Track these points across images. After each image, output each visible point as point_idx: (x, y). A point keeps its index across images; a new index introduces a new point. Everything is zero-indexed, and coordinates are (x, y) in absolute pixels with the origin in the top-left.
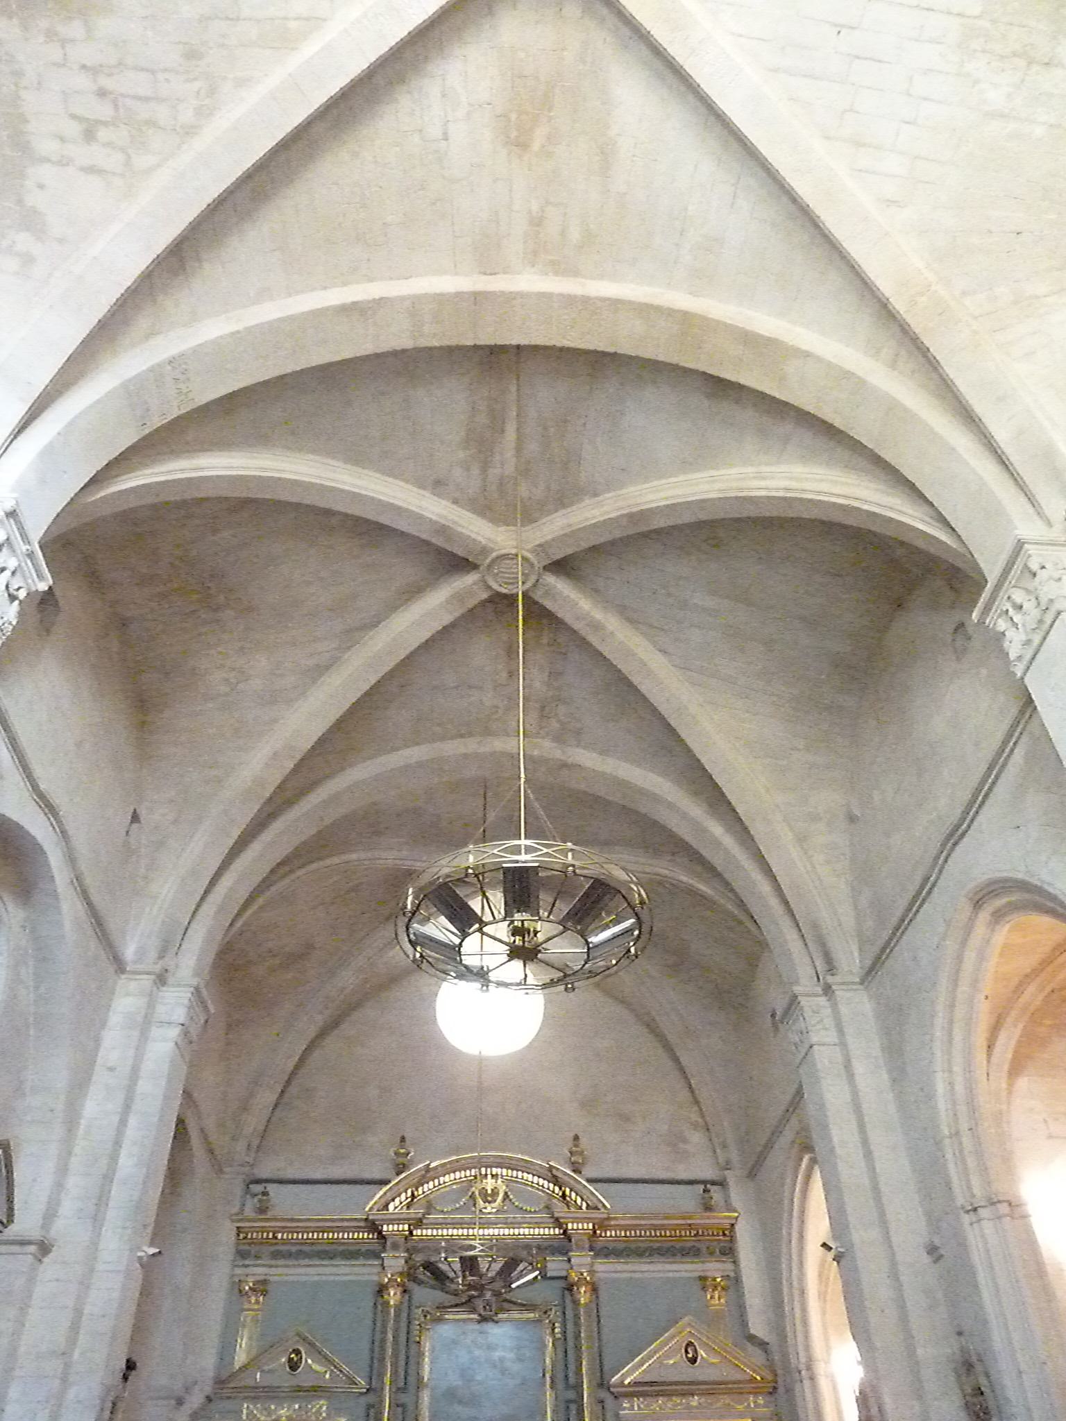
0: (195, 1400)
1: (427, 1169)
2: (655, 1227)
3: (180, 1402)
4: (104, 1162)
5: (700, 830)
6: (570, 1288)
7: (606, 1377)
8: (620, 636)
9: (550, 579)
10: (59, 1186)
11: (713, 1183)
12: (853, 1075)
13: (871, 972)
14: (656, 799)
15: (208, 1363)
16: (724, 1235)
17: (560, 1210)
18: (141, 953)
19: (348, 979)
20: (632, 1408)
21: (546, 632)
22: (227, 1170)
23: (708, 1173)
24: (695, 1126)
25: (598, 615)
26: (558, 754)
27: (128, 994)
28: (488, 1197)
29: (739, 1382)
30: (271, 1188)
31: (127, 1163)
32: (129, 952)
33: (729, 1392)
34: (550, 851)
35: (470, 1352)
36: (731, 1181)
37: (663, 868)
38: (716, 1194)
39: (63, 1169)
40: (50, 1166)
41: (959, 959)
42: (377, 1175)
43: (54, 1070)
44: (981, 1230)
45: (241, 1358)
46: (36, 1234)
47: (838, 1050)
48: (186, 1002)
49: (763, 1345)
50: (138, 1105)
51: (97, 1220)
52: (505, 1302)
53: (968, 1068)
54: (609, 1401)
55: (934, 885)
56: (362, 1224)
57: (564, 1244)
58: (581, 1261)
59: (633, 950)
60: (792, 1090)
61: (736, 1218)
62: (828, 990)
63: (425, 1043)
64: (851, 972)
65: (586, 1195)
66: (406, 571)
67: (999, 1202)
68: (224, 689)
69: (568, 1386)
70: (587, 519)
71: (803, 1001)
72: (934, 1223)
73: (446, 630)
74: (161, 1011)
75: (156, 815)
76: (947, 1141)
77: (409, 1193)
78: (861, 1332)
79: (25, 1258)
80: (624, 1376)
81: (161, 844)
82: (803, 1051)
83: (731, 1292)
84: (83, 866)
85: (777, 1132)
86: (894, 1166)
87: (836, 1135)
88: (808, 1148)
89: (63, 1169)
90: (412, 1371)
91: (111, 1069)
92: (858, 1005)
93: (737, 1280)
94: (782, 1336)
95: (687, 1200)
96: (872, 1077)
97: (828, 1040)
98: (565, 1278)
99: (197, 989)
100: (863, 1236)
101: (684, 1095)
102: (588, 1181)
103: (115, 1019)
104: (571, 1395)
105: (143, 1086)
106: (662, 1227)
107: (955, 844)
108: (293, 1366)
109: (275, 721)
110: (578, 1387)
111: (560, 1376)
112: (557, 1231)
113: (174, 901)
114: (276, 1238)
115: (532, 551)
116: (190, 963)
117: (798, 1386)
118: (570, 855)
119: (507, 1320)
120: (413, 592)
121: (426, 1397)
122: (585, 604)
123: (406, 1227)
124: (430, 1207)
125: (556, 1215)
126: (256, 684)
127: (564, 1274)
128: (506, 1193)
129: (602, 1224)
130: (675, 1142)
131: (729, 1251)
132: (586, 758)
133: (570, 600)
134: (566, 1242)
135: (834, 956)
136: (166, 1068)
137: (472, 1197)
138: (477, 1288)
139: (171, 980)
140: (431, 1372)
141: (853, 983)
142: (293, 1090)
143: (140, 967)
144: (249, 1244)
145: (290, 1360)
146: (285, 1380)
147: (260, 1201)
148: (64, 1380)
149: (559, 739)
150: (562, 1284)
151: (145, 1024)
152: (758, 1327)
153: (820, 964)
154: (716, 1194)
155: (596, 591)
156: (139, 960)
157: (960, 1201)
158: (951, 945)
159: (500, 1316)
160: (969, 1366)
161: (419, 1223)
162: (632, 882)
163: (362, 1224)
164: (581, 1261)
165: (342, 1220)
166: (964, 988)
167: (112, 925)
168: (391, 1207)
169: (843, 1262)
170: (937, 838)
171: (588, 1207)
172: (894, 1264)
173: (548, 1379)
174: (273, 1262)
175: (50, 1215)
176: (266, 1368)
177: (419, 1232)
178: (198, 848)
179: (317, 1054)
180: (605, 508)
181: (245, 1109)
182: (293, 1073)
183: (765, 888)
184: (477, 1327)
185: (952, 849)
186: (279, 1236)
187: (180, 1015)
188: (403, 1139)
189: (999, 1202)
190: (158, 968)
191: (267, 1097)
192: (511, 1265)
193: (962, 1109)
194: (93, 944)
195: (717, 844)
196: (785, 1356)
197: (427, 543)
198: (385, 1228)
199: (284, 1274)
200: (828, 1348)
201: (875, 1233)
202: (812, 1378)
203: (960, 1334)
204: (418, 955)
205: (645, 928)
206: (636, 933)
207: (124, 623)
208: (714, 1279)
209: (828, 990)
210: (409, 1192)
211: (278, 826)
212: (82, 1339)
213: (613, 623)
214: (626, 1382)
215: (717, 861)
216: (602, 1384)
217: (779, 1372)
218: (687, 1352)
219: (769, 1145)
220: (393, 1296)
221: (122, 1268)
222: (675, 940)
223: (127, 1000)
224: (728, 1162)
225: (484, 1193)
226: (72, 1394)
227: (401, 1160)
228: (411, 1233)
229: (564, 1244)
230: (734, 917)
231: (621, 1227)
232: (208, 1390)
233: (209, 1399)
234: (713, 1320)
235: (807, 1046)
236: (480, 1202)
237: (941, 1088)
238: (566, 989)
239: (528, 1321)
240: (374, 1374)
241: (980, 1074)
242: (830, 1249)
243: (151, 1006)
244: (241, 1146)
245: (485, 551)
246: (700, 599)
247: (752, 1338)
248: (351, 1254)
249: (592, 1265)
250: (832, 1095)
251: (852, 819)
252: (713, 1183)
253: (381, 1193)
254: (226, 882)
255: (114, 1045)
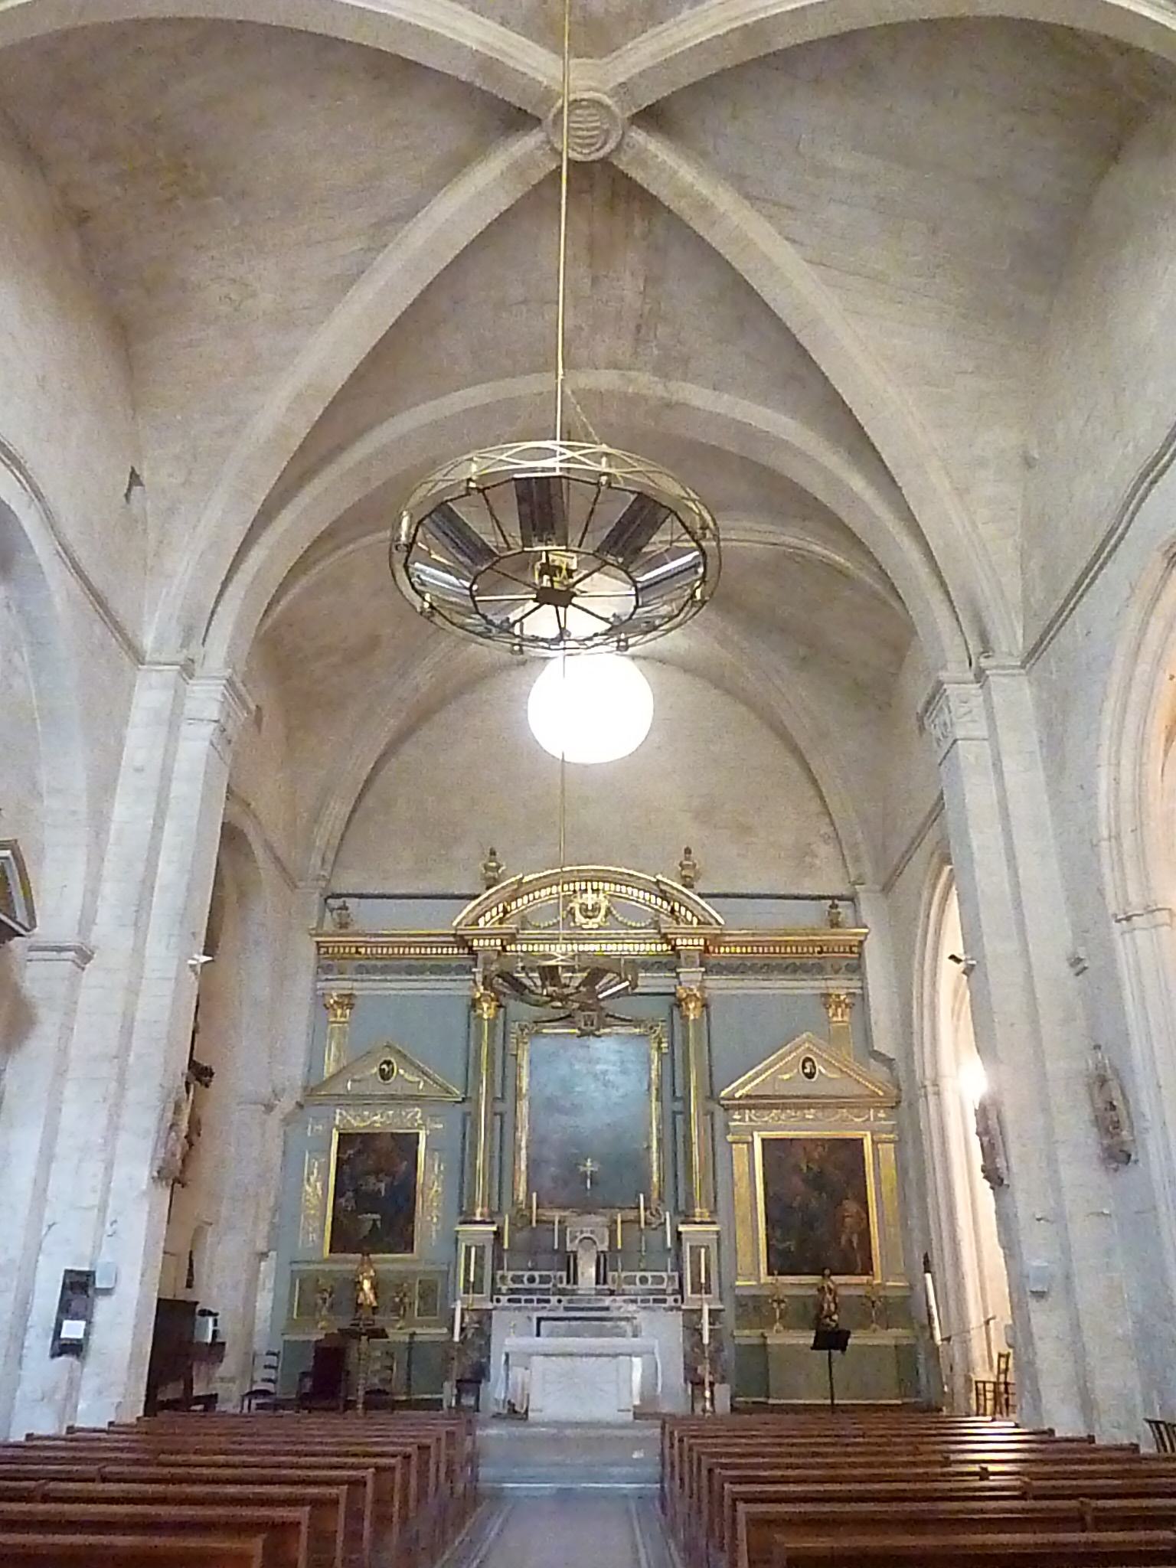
0: (286, 1104)
1: (520, 882)
2: (776, 943)
3: (269, 1108)
4: (140, 867)
5: (834, 482)
6: (679, 1003)
7: (716, 1090)
8: (735, 219)
9: (638, 136)
10: (92, 893)
11: (841, 898)
12: (1002, 773)
13: (1034, 653)
14: (782, 445)
15: (293, 1072)
16: (852, 952)
17: (668, 925)
18: (161, 641)
19: (423, 677)
20: (742, 1120)
21: (638, 221)
22: (301, 884)
23: (841, 889)
24: (826, 839)
25: (703, 188)
26: (660, 390)
27: (151, 687)
28: (590, 912)
29: (859, 1096)
30: (351, 903)
31: (167, 870)
32: (148, 642)
33: (850, 1106)
34: (576, 454)
35: (571, 1065)
36: (862, 896)
37: (791, 537)
38: (844, 909)
39: (95, 878)
40: (80, 869)
41: (1144, 626)
42: (467, 892)
43: (67, 770)
44: (1133, 939)
45: (330, 1068)
46: (73, 940)
47: (989, 750)
48: (220, 697)
49: (888, 1062)
50: (173, 808)
51: (139, 925)
52: (608, 1019)
53: (1139, 763)
54: (720, 1114)
55: (1121, 538)
56: (452, 939)
57: (672, 961)
58: (691, 976)
59: (698, 593)
60: (937, 794)
61: (866, 934)
62: (980, 676)
63: (517, 752)
64: (1011, 654)
65: (698, 911)
66: (449, 133)
67: (1159, 910)
68: (225, 309)
69: (674, 1098)
70: (685, 40)
71: (950, 689)
72: (1081, 932)
73: (504, 221)
74: (191, 707)
75: (159, 475)
76: (1104, 844)
77: (501, 908)
78: (985, 1043)
79: (64, 966)
80: (737, 1089)
81: (172, 511)
82: (945, 747)
83: (857, 1008)
84: (71, 535)
85: (914, 844)
86: (1041, 874)
87: (976, 841)
88: (946, 859)
89: (95, 878)
90: (509, 1082)
91: (139, 770)
92: (1014, 693)
93: (864, 998)
94: (909, 1055)
95: (811, 915)
96: (1024, 774)
97: (977, 734)
98: (673, 994)
99: (230, 682)
100: (998, 947)
101: (815, 806)
102: (701, 896)
103: (137, 716)
104: (678, 1106)
105: (177, 789)
106: (787, 943)
107: (1154, 482)
108: (385, 1076)
109: (296, 351)
110: (686, 1100)
111: (667, 1088)
112: (665, 947)
113: (194, 576)
114: (357, 952)
115: (613, 93)
116: (219, 650)
117: (922, 1100)
118: (604, 460)
119: (609, 1035)
120: (457, 165)
121: (524, 1106)
122: (688, 174)
123: (499, 942)
124: (524, 923)
125: (663, 931)
126: (266, 300)
127: (673, 990)
128: (608, 909)
129: (715, 940)
130: (803, 855)
131: (857, 968)
132: (698, 396)
133: (664, 165)
134: (674, 959)
135: (992, 637)
136: (201, 768)
137: (571, 912)
138: (581, 1000)
139: (198, 672)
140: (529, 1084)
141: (1014, 667)
142: (370, 801)
143: (157, 657)
144: (332, 959)
145: (382, 1071)
146: (381, 1089)
147: (339, 915)
148: (121, 1082)
149: (661, 370)
150: (672, 999)
151: (173, 722)
152: (883, 1043)
153: (974, 646)
154: (844, 909)
155: (704, 154)
156: (158, 650)
157: (1112, 908)
158: (1134, 616)
159: (602, 1031)
160: (1103, 1081)
161: (513, 938)
162: (690, 499)
163: (452, 939)
164: (691, 976)
165: (429, 935)
166: (1143, 668)
167: (120, 606)
168: (481, 921)
169: (973, 975)
170: (1133, 475)
171: (699, 923)
172: (1029, 976)
173: (654, 1092)
174: (359, 977)
175: (87, 921)
176: (356, 1077)
177: (513, 947)
178: (221, 516)
179: (394, 763)
180: (710, 22)
181: (315, 821)
182: (368, 782)
183: (913, 554)
184: (577, 1040)
185: (1149, 489)
186: (363, 950)
187: (213, 711)
188: (493, 853)
189: (1159, 910)
190: (181, 658)
191: (339, 809)
192: (595, 975)
193: (1127, 808)
194: (98, 629)
195: (855, 499)
196: (911, 1072)
197: (468, 88)
198: (475, 943)
199: (364, 988)
200: (958, 1064)
201: (1013, 946)
202: (938, 1094)
203: (1097, 1047)
204: (426, 605)
205: (712, 562)
206: (701, 570)
207: (82, 218)
208: (838, 996)
209: (980, 676)
210: (501, 907)
211: (314, 488)
212: (136, 1043)
213: (724, 199)
214: (737, 1095)
215: (856, 524)
216: (712, 1096)
217: (904, 1086)
218: (804, 1067)
219: (906, 857)
220: (487, 1010)
221: (172, 974)
222: (821, 640)
223: (150, 695)
224: (860, 876)
225: (584, 910)
226: (131, 1095)
227: (491, 874)
228: (504, 949)
229: (672, 961)
230: (874, 594)
231: (737, 944)
232: (298, 1097)
233: (300, 1106)
234: (833, 1038)
235: (950, 741)
236: (579, 918)
237: (1104, 785)
238: (618, 648)
239: (634, 1035)
240: (469, 1083)
241: (1154, 769)
242: (958, 961)
243: (178, 700)
244: (316, 860)
245: (548, 96)
246: (842, 161)
247: (877, 1056)
248: (440, 969)
249: (703, 980)
250: (976, 797)
251: (1028, 462)
252: (841, 898)
253: (469, 907)
254: (257, 555)
255: (140, 743)
